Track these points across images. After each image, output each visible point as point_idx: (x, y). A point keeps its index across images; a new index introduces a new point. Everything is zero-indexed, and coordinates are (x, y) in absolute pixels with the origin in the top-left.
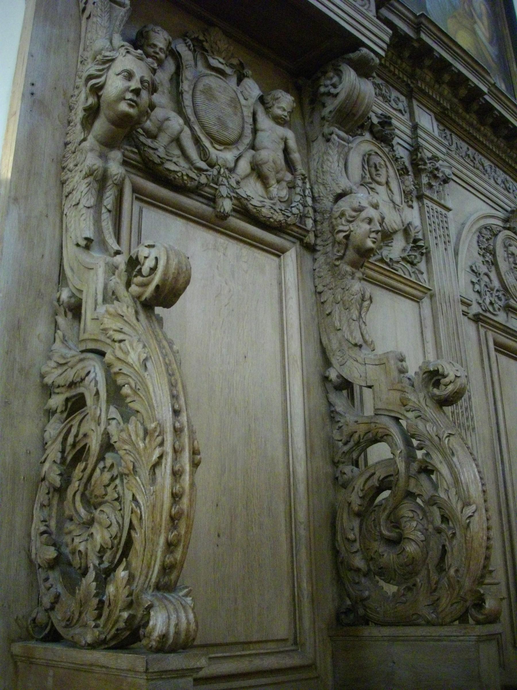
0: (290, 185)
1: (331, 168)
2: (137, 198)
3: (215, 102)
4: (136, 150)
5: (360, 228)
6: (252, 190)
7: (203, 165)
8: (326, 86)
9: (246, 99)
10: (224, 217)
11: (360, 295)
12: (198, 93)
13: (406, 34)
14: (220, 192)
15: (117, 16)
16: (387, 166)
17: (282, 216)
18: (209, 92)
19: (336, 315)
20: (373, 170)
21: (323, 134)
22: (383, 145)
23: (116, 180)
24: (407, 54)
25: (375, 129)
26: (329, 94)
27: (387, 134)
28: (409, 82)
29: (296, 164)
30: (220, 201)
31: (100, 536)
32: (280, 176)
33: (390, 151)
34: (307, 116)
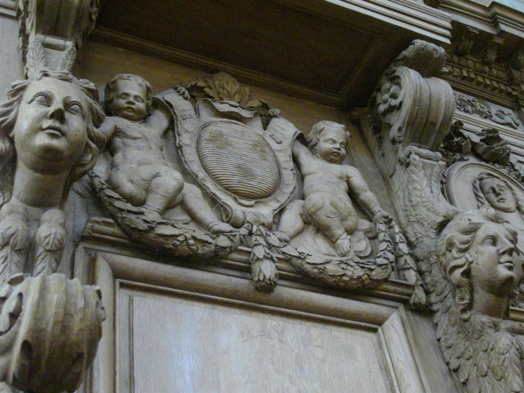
0: (370, 235)
1: (421, 197)
2: (122, 285)
3: (231, 149)
4: (111, 221)
5: (482, 253)
6: (314, 250)
7: (226, 227)
8: (385, 102)
9: (280, 143)
10: (267, 287)
11: (513, 350)
12: (204, 143)
13: (481, 31)
14: (254, 255)
15: (57, 61)
16: (511, 188)
17: (360, 270)
18: (218, 139)
20: (492, 196)
21: (400, 161)
22: (497, 165)
23: (48, 244)
24: (492, 56)
25: (480, 150)
26: (392, 109)
27: (498, 150)
28: (510, 90)
29: (371, 206)
30: (256, 267)
32: (350, 223)
33: (510, 171)
34: (376, 151)
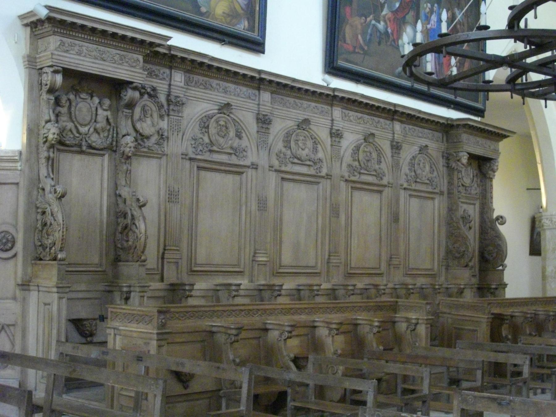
19: (120, 174)
31: (50, 241)
